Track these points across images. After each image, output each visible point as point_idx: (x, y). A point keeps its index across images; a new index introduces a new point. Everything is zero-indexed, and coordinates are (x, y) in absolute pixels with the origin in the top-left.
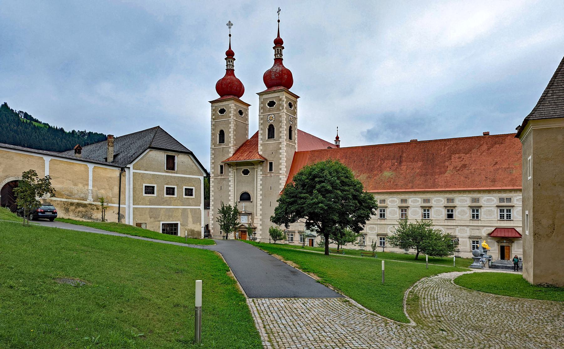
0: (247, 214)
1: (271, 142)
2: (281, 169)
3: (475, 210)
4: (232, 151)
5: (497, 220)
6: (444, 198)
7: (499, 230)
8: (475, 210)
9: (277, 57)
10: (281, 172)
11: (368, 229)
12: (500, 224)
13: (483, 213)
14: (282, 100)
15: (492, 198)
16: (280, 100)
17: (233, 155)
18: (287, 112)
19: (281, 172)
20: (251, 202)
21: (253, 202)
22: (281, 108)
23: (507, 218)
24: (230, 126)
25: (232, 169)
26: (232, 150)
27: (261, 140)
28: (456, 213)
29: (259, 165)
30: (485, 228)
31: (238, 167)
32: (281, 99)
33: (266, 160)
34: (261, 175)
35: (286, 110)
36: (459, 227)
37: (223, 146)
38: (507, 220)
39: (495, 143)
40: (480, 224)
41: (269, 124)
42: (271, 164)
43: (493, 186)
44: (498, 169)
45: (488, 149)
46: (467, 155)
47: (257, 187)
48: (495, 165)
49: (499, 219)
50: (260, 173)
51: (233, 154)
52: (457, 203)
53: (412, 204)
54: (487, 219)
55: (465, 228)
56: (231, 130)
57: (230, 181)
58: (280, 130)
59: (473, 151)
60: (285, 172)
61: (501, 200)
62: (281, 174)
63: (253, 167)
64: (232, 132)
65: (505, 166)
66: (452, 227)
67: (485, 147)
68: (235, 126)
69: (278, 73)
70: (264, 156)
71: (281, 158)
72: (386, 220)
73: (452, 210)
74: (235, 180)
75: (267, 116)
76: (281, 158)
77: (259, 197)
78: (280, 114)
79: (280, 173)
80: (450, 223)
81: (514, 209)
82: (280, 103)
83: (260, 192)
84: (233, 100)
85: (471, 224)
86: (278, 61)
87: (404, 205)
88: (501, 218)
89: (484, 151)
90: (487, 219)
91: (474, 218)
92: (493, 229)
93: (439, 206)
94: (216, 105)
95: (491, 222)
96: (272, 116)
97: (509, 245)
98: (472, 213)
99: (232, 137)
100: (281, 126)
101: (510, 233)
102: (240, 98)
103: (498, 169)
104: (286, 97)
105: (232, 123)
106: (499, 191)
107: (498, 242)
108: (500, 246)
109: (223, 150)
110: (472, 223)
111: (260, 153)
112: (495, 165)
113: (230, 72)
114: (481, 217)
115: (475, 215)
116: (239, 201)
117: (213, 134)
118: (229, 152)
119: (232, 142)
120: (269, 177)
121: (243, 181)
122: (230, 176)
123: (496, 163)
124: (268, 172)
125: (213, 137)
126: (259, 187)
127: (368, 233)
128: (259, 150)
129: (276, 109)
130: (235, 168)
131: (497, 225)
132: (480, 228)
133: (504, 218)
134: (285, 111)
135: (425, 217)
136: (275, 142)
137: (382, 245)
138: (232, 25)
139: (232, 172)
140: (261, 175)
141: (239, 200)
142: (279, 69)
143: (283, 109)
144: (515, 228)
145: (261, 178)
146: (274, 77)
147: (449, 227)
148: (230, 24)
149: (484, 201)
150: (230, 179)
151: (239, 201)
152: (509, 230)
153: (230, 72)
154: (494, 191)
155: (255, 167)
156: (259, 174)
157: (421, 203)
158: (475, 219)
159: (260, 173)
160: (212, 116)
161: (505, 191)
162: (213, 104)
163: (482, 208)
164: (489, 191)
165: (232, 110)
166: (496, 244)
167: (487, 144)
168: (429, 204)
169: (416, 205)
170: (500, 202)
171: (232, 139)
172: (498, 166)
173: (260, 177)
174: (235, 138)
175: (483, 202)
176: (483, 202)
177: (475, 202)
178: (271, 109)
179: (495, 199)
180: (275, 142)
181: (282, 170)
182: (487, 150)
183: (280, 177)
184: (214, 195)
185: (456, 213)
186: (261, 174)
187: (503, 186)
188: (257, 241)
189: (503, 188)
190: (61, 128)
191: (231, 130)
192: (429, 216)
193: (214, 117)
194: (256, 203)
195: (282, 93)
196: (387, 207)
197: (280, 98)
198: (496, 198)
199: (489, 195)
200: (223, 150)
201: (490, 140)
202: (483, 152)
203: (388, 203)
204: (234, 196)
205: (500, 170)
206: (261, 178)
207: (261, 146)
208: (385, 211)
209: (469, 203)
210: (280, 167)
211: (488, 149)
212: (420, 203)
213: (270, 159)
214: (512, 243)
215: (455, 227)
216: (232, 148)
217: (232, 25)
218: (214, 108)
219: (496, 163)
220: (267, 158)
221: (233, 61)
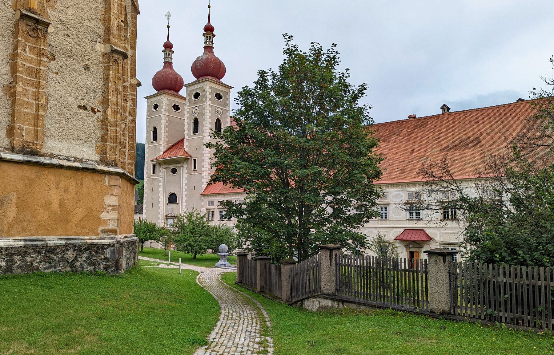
0: (173, 217)
1: (196, 137)
2: (203, 166)
3: (384, 208)
4: (163, 149)
5: (405, 219)
7: (407, 232)
8: (384, 208)
9: (206, 45)
10: (203, 169)
12: (409, 224)
13: (391, 212)
14: (205, 90)
16: (204, 90)
17: (163, 153)
19: (203, 169)
20: (178, 204)
21: (179, 204)
22: (204, 100)
23: (417, 218)
24: (161, 122)
25: (162, 169)
26: (163, 147)
27: (187, 135)
29: (185, 163)
30: (394, 230)
31: (167, 166)
32: (205, 90)
33: (191, 156)
34: (186, 173)
35: (210, 102)
37: (156, 143)
38: (416, 220)
39: (416, 128)
40: (388, 226)
41: (194, 117)
42: (195, 160)
43: (402, 178)
44: (413, 158)
45: (408, 135)
46: (386, 143)
47: (182, 187)
48: (411, 153)
50: (185, 171)
51: (163, 152)
54: (396, 218)
56: (162, 126)
57: (160, 181)
58: (203, 124)
59: (392, 138)
60: (207, 169)
61: (410, 195)
62: (203, 171)
63: (179, 165)
64: (163, 129)
65: (422, 154)
67: (405, 132)
68: (167, 122)
69: (203, 62)
70: (189, 153)
71: (204, 154)
73: (386, 208)
74: (164, 180)
75: (192, 109)
76: (204, 154)
77: (185, 198)
78: (204, 106)
79: (203, 170)
81: (390, 207)
82: (204, 94)
83: (185, 193)
84: (164, 94)
85: (379, 226)
86: (209, 49)
89: (403, 137)
90: (396, 218)
91: (383, 218)
92: (402, 231)
94: (151, 100)
95: (400, 222)
96: (197, 108)
97: (418, 251)
99: (163, 134)
100: (204, 119)
102: (221, 80)
103: (413, 158)
104: (211, 88)
105: (163, 118)
106: (408, 184)
107: (407, 247)
108: (408, 252)
109: (155, 147)
110: (380, 224)
111: (186, 149)
112: (411, 153)
113: (168, 64)
114: (390, 217)
115: (384, 213)
116: (167, 203)
117: (148, 132)
119: (163, 139)
120: (193, 176)
121: (171, 181)
122: (160, 176)
123: (413, 151)
124: (192, 170)
125: (148, 135)
126: (185, 187)
128: (185, 147)
129: (200, 100)
130: (164, 167)
131: (405, 226)
132: (389, 230)
133: (413, 218)
134: (209, 102)
135: (383, 218)
136: (199, 137)
138: (171, 15)
139: (162, 171)
140: (186, 173)
141: (167, 201)
142: (208, 55)
143: (206, 100)
144: (425, 230)
145: (186, 177)
146: (199, 66)
148: (168, 15)
149: (393, 197)
150: (160, 179)
151: (167, 203)
152: (411, 232)
153: (168, 64)
154: (403, 184)
155: (182, 165)
156: (184, 171)
158: (384, 219)
159: (185, 171)
160: (147, 113)
161: (414, 184)
162: (148, 100)
163: (390, 205)
164: (397, 185)
165: (164, 104)
166: (405, 249)
167: (408, 129)
171: (163, 136)
172: (413, 155)
173: (185, 176)
174: (167, 134)
175: (391, 198)
176: (391, 198)
179: (404, 194)
180: (199, 137)
181: (204, 167)
182: (407, 136)
183: (203, 175)
184: (147, 197)
186: (187, 172)
187: (411, 178)
189: (411, 181)
191: (162, 126)
192: (387, 216)
193: (149, 114)
194: (182, 204)
195: (206, 83)
197: (204, 88)
198: (404, 193)
199: (397, 189)
200: (155, 147)
201: (412, 124)
202: (402, 139)
204: (164, 198)
205: (415, 159)
206: (186, 177)
207: (187, 142)
208: (388, 209)
209: (405, 198)
210: (203, 165)
211: (408, 135)
213: (194, 156)
214: (421, 248)
216: (163, 145)
217: (171, 15)
218: (149, 104)
219: (413, 151)
220: (192, 155)
221: (212, 36)
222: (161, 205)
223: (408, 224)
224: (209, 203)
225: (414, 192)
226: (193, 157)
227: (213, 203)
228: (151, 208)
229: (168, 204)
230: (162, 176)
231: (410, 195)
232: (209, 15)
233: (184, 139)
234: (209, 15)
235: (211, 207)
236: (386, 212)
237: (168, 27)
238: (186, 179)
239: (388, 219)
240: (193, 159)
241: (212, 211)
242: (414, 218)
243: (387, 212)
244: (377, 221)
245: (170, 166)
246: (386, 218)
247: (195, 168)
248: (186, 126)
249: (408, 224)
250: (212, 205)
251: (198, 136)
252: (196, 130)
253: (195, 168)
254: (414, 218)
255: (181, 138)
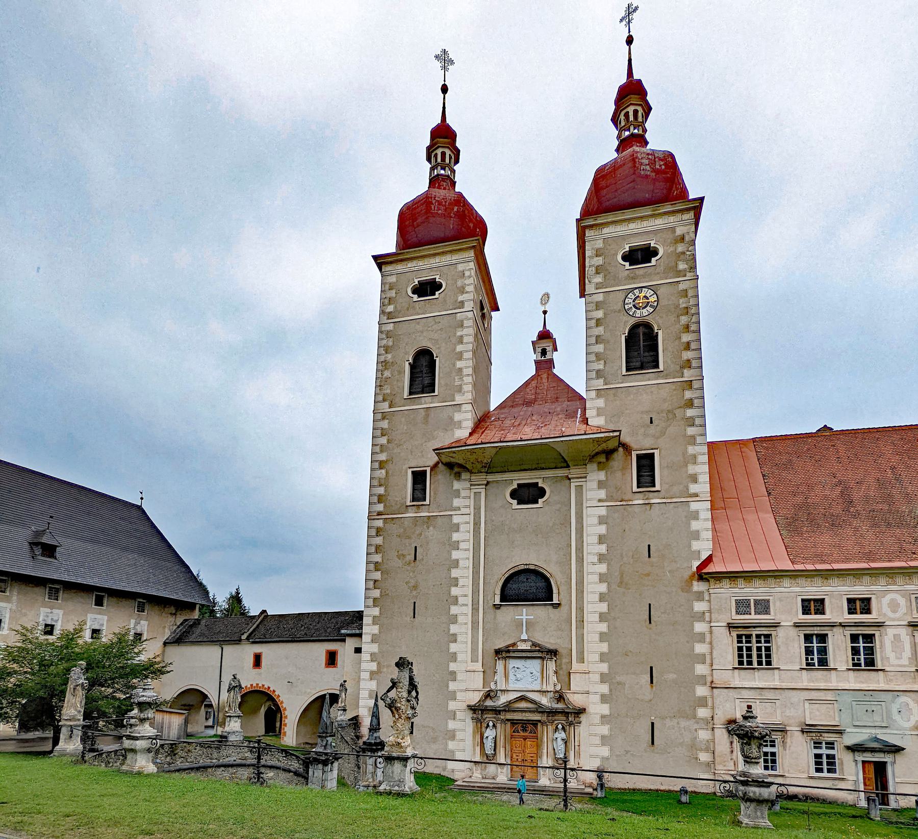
21: (564, 608)
31: (491, 478)
40: (777, 684)
61: (742, 606)
77: (594, 588)
151: (498, 602)
158: (764, 666)
183: (456, 520)
200: (427, 416)
222: (462, 611)
225: (752, 599)
226: (633, 445)
228: (409, 618)
229: (497, 607)
231: (742, 606)
232: (630, 60)
234: (630, 60)
237: (444, 89)
240: (634, 454)
242: (755, 665)
243: (736, 645)
246: (769, 663)
251: (657, 379)
254: (755, 665)
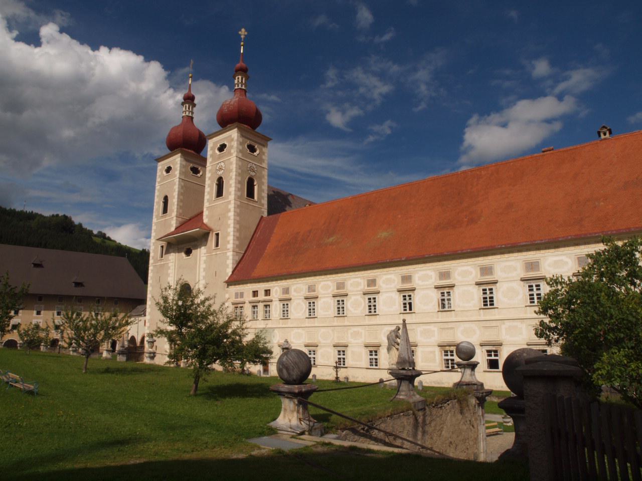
6: (363, 278)
11: (349, 335)
13: (319, 309)
15: (564, 258)
18: (243, 157)
28: (417, 300)
34: (205, 254)
36: (508, 323)
40: (316, 325)
41: (218, 177)
42: (217, 235)
49: (529, 304)
51: (175, 228)
52: (498, 274)
53: (420, 283)
55: (517, 324)
66: (494, 324)
72: (346, 318)
80: (491, 314)
87: (407, 286)
88: (485, 305)
93: (467, 283)
96: (222, 164)
98: (528, 293)
101: (43, 348)
118: (171, 226)
127: (351, 344)
129: (227, 153)
135: (487, 305)
137: (373, 365)
140: (205, 254)
147: (446, 326)
149: (567, 263)
156: (201, 253)
157: (364, 286)
168: (449, 281)
169: (427, 285)
170: (441, 279)
177: (487, 274)
178: (222, 155)
185: (498, 297)
188: (157, 363)
190: (31, 212)
196: (495, 283)
203: (381, 284)
212: (433, 280)
215: (498, 323)
223: (281, 323)
224: (237, 295)
227: (242, 295)
230: (172, 261)
233: (202, 213)
235: (239, 300)
236: (491, 295)
238: (205, 262)
239: (495, 306)
241: (241, 307)
244: (523, 309)
245: (183, 246)
247: (217, 245)
248: (207, 189)
249: (281, 323)
250: (241, 298)
252: (220, 193)
253: (217, 245)
255: (200, 211)
